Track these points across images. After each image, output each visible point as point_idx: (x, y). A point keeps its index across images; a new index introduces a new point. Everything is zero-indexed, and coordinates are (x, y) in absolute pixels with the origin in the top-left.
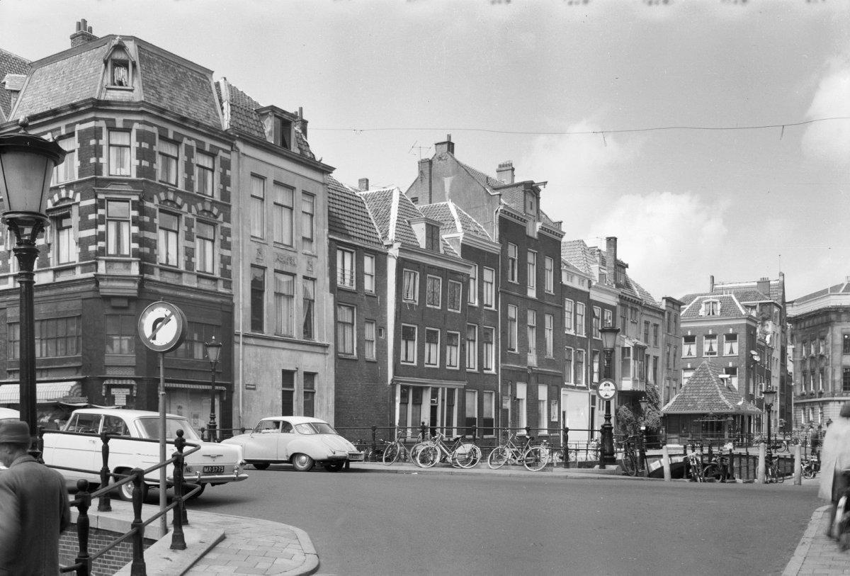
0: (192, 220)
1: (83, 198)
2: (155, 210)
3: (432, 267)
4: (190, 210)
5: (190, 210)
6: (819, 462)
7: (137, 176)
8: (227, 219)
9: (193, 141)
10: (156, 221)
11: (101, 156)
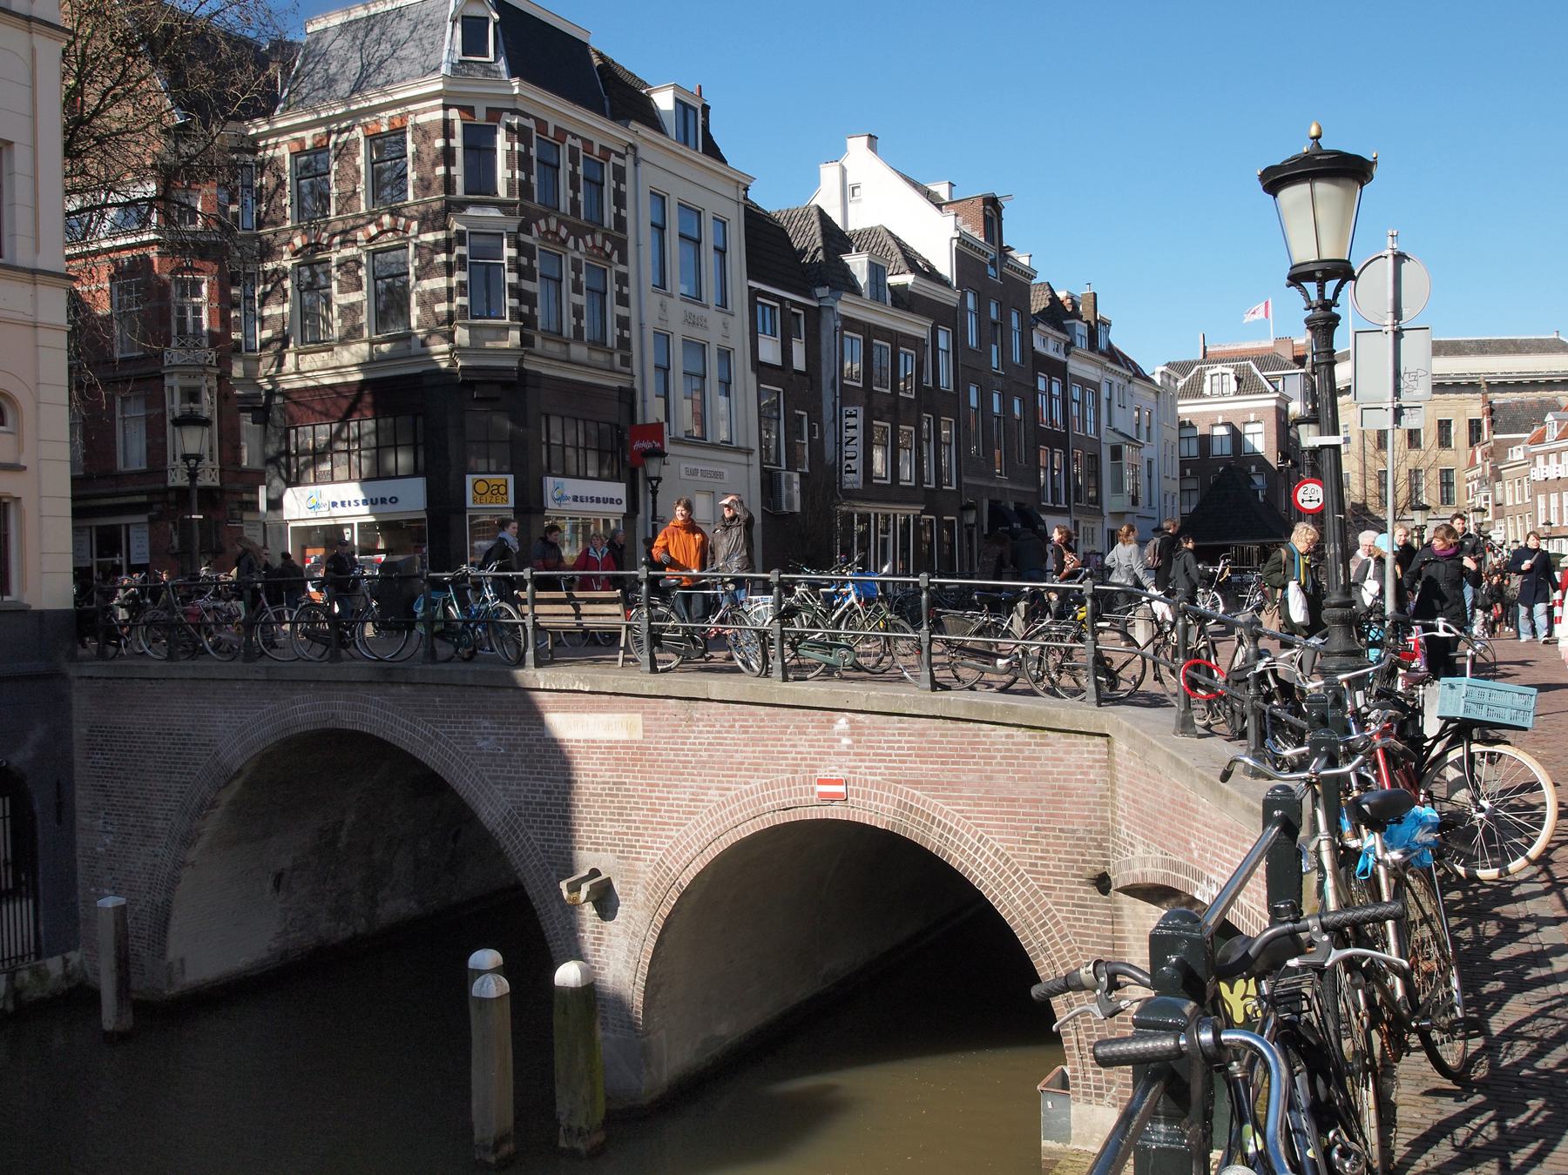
0: (580, 261)
3: (877, 327)
8: (623, 260)
10: (536, 264)
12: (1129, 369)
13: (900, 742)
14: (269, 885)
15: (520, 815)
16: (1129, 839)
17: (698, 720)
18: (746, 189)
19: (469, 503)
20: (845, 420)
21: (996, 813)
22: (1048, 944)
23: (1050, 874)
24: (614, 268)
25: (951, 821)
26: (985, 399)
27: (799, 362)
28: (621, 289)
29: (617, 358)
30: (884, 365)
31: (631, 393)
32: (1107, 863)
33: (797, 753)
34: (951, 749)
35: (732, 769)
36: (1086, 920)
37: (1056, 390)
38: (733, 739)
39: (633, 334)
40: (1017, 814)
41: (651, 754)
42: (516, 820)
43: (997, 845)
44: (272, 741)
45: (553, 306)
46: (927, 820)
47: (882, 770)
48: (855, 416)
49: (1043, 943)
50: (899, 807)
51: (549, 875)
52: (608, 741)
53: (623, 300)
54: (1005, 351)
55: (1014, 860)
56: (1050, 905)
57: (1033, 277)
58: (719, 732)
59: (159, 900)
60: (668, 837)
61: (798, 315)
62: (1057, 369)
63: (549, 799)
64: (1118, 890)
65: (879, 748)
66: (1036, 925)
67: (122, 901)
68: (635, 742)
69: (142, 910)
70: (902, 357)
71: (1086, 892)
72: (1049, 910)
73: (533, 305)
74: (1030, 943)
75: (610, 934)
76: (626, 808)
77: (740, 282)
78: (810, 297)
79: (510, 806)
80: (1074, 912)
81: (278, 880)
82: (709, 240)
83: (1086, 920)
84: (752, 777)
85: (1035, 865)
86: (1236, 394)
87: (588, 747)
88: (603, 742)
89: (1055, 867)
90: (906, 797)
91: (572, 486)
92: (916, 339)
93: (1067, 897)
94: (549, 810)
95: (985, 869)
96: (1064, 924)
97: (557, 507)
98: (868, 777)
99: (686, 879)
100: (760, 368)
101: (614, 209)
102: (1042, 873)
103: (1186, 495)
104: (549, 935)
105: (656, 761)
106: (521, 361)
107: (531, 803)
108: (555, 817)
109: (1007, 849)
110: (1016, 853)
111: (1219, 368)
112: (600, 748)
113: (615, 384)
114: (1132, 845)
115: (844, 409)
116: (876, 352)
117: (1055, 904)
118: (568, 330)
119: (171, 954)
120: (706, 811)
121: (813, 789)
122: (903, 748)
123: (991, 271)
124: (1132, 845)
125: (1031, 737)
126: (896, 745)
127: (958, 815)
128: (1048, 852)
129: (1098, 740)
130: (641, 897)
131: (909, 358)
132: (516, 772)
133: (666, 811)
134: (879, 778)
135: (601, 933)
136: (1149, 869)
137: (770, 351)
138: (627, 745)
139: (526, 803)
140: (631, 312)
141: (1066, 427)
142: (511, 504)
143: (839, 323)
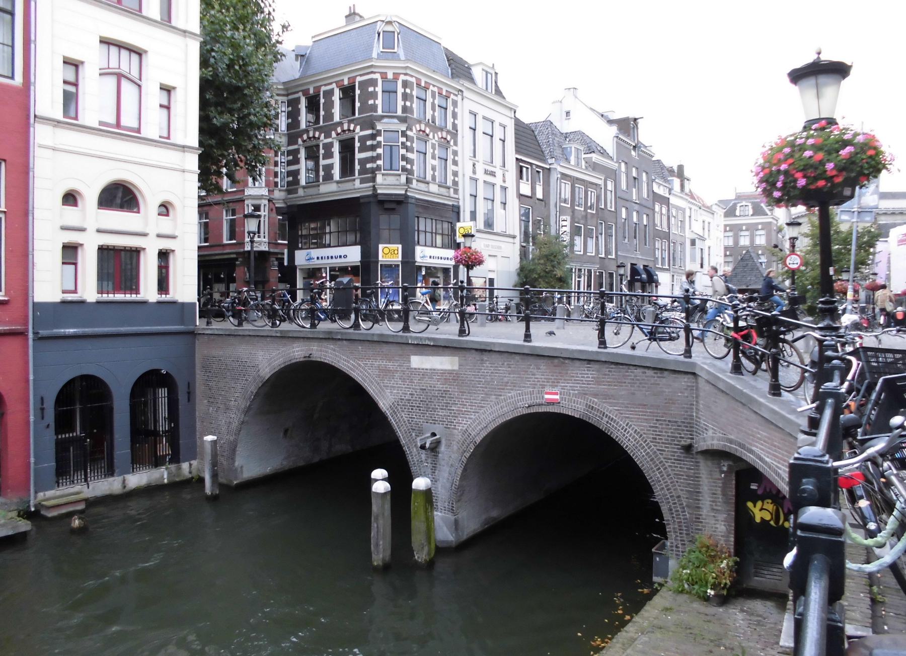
0: (435, 144)
1: (361, 130)
2: (413, 137)
3: (577, 179)
4: (434, 137)
5: (434, 137)
6: (659, 590)
7: (402, 113)
8: (456, 144)
10: (414, 145)
11: (377, 99)
12: (699, 202)
13: (588, 374)
14: (282, 434)
15: (398, 405)
16: (705, 427)
17: (486, 361)
18: (515, 112)
20: (561, 223)
21: (636, 411)
22: (660, 479)
23: (663, 443)
24: (451, 148)
25: (613, 415)
26: (629, 214)
27: (539, 195)
28: (454, 158)
29: (452, 190)
30: (581, 197)
31: (458, 207)
33: (535, 378)
34: (613, 378)
35: (502, 385)
36: (681, 468)
37: (664, 211)
38: (503, 370)
39: (459, 179)
40: (647, 412)
41: (462, 377)
42: (396, 407)
43: (636, 428)
44: (283, 366)
45: (422, 165)
46: (600, 414)
47: (578, 388)
48: (566, 221)
51: (412, 434)
52: (442, 370)
53: (455, 163)
54: (639, 191)
55: (645, 435)
56: (662, 459)
58: (497, 367)
59: (232, 438)
60: (470, 418)
62: (665, 201)
63: (412, 397)
65: (577, 377)
66: (655, 469)
67: (215, 438)
68: (454, 370)
69: (224, 443)
70: (589, 193)
71: (681, 453)
72: (662, 462)
73: (412, 165)
75: (440, 465)
76: (449, 403)
77: (511, 155)
78: (546, 164)
79: (393, 400)
80: (674, 463)
81: (286, 431)
83: (681, 468)
84: (512, 390)
85: (656, 439)
86: (752, 215)
87: (432, 373)
88: (438, 370)
89: (666, 440)
90: (590, 402)
92: (596, 185)
93: (672, 455)
94: (412, 403)
95: (629, 440)
96: (669, 469)
97: (421, 261)
98: (571, 392)
99: (478, 440)
100: (521, 196)
102: (659, 443)
104: (411, 464)
105: (465, 380)
106: (406, 191)
107: (403, 399)
108: (414, 406)
109: (641, 430)
110: (645, 432)
111: (744, 203)
112: (437, 373)
113: (450, 203)
114: (706, 429)
115: (561, 217)
117: (665, 458)
119: (236, 464)
120: (489, 406)
122: (589, 378)
125: (655, 373)
126: (586, 376)
127: (617, 412)
128: (662, 432)
129: (690, 376)
130: (455, 448)
131: (593, 193)
132: (397, 384)
133: (469, 405)
134: (576, 392)
135: (436, 464)
136: (715, 442)
137: (526, 189)
138: (450, 372)
139: (401, 399)
142: (400, 259)
143: (559, 176)
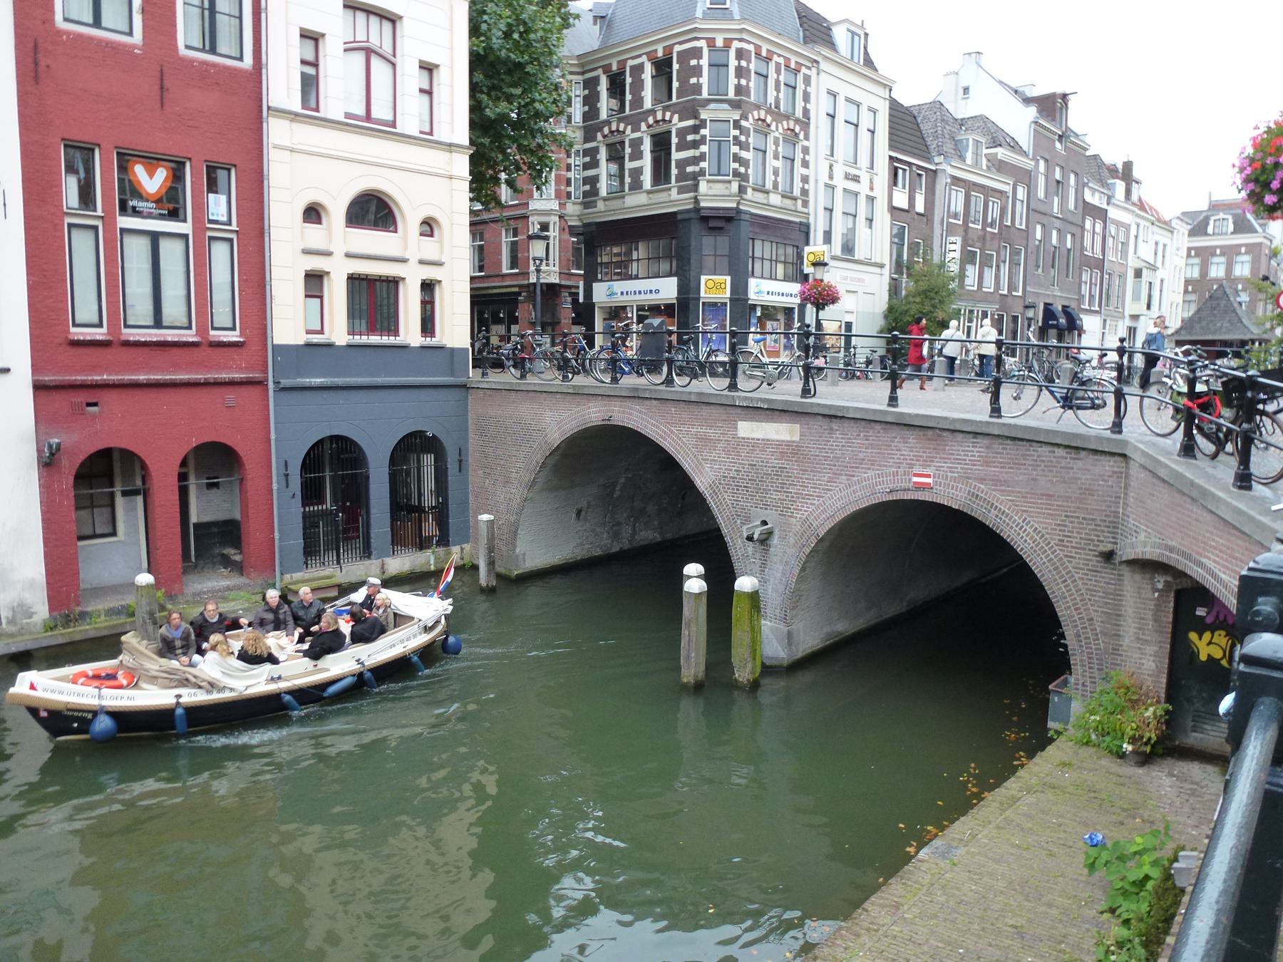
3: (975, 184)
8: (807, 138)
9: (752, 46)
10: (751, 140)
12: (1153, 215)
14: (574, 515)
18: (890, 90)
19: (702, 294)
20: (948, 246)
22: (1067, 594)
26: (1046, 234)
27: (920, 208)
29: (799, 202)
31: (808, 226)
32: (1116, 543)
37: (1098, 228)
39: (810, 187)
49: (1063, 593)
50: (968, 494)
53: (805, 164)
55: (1048, 536)
57: (1086, 149)
59: (512, 519)
61: (920, 175)
62: (1101, 214)
64: (1122, 563)
66: (1059, 581)
67: (492, 517)
68: (793, 442)
70: (991, 203)
71: (1098, 561)
73: (747, 167)
74: (1054, 592)
77: (883, 151)
78: (930, 163)
81: (579, 513)
82: (866, 122)
84: (869, 469)
91: (768, 285)
92: (1001, 192)
95: (1026, 541)
99: (822, 532)
101: (803, 104)
103: (1187, 305)
106: (738, 203)
111: (1221, 216)
114: (1136, 532)
116: (973, 199)
117: (1074, 568)
118: (769, 185)
121: (910, 480)
123: (1058, 145)
124: (1136, 532)
136: (1148, 549)
137: (901, 200)
138: (788, 444)
140: (809, 172)
141: (1104, 255)
142: (728, 295)
143: (949, 180)
